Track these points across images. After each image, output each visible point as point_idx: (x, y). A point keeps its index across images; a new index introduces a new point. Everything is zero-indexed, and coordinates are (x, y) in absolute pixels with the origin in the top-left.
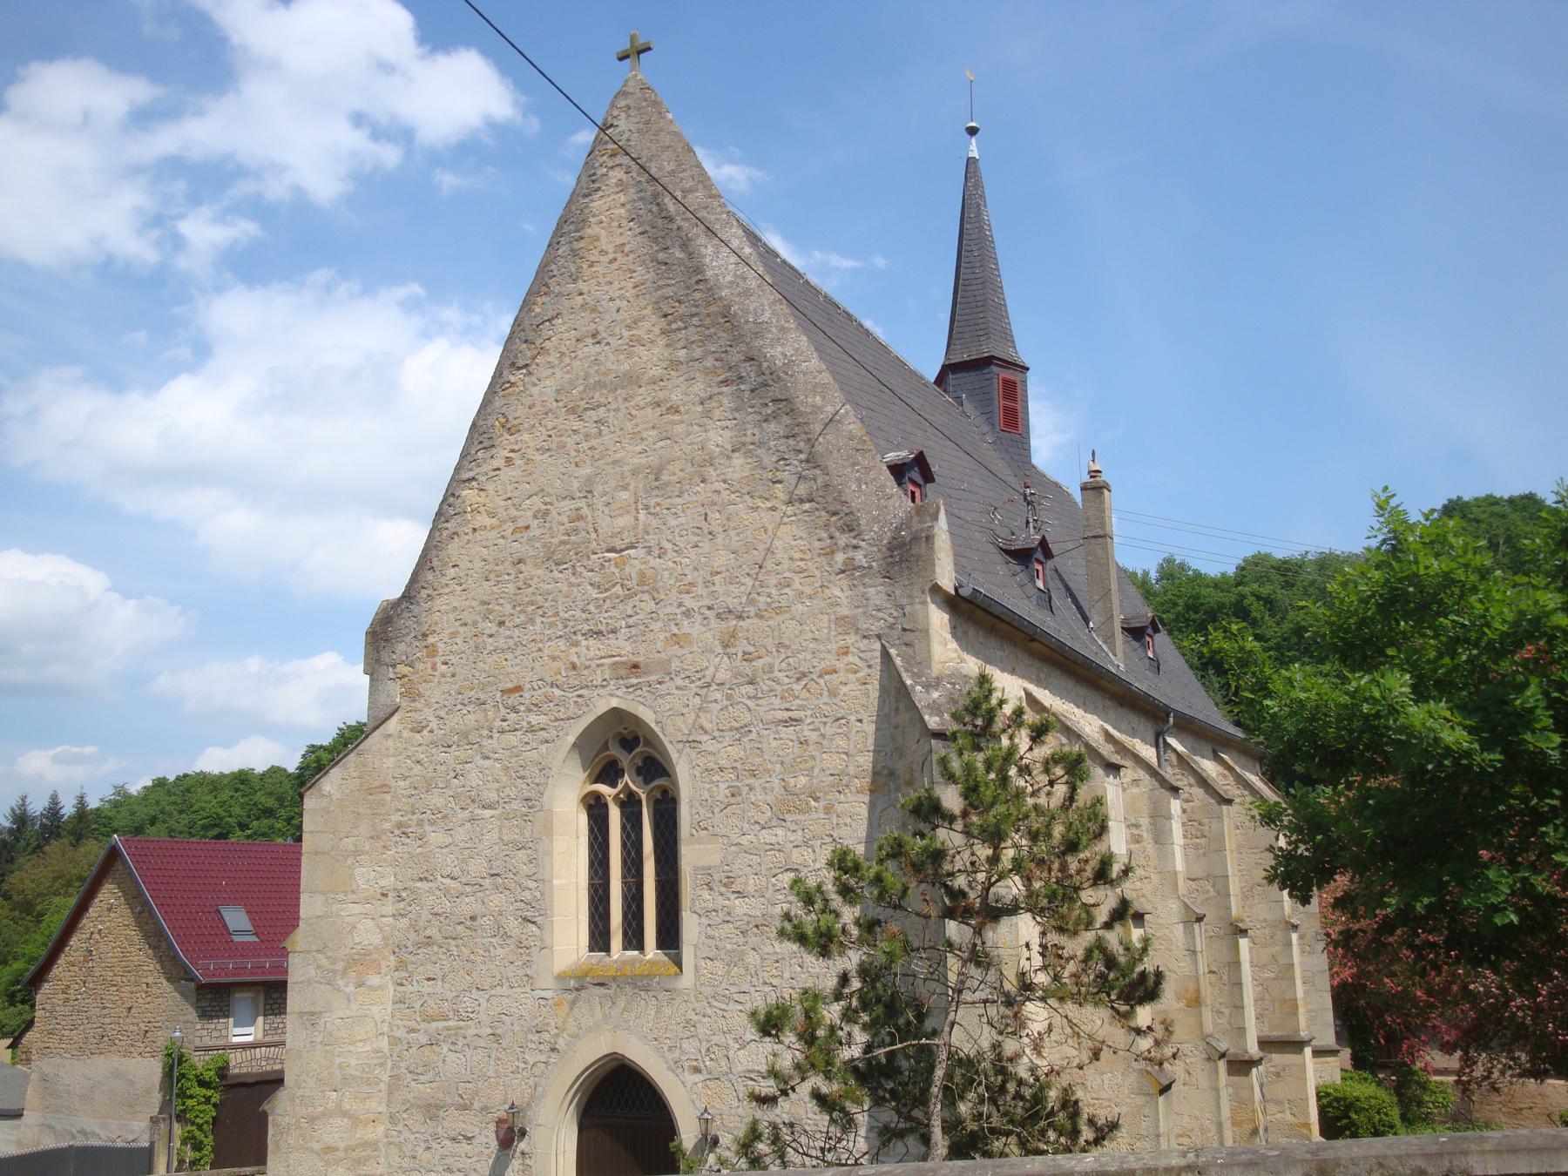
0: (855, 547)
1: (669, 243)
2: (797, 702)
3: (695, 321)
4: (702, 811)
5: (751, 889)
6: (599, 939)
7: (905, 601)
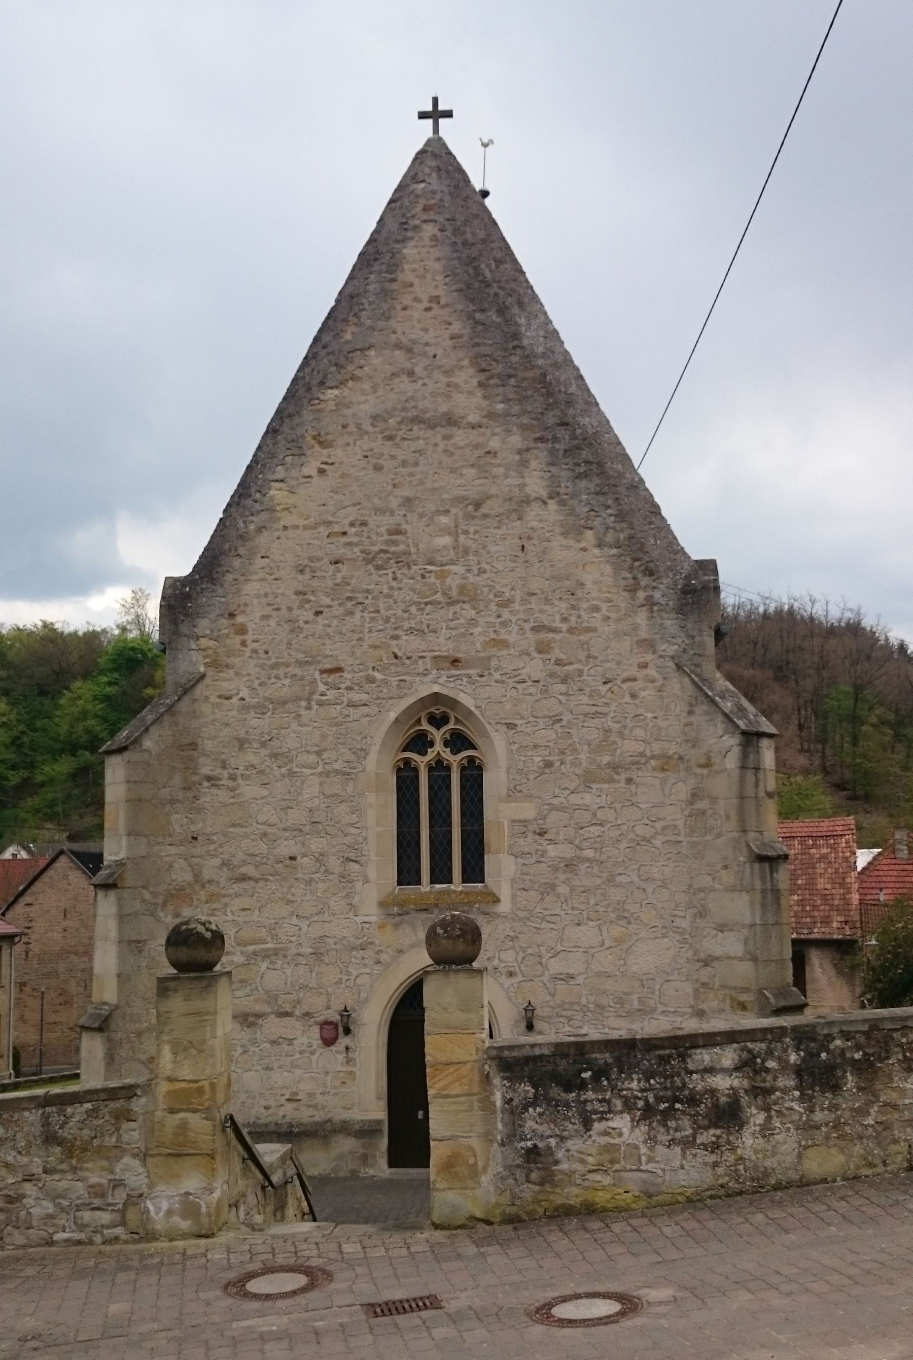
0: (654, 588)
1: (486, 306)
2: (603, 700)
3: (512, 381)
4: (518, 778)
5: (561, 838)
6: (407, 873)
7: (695, 633)
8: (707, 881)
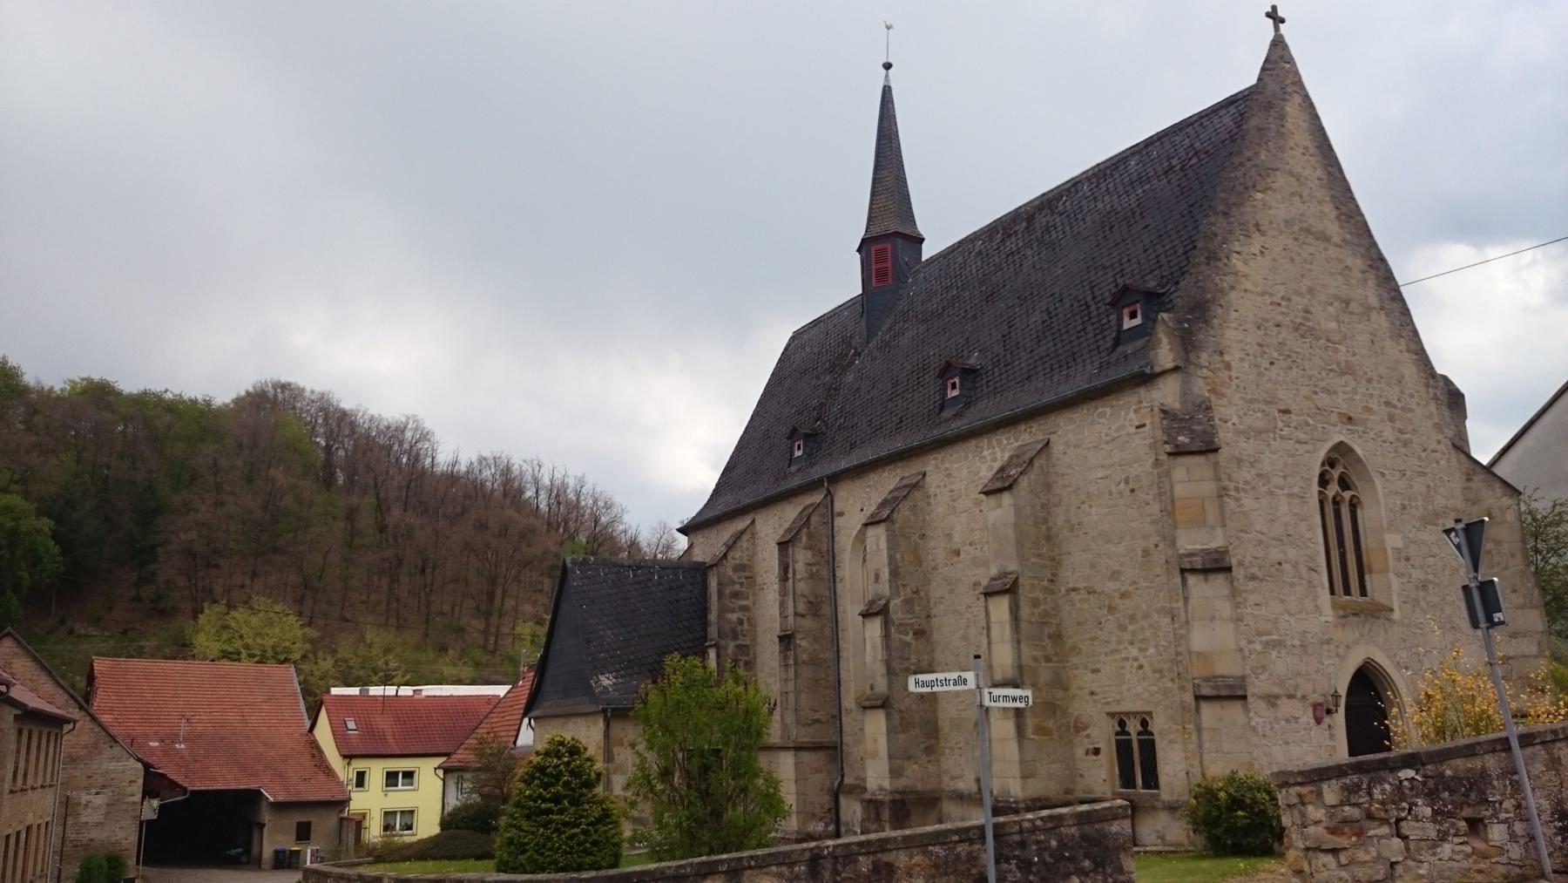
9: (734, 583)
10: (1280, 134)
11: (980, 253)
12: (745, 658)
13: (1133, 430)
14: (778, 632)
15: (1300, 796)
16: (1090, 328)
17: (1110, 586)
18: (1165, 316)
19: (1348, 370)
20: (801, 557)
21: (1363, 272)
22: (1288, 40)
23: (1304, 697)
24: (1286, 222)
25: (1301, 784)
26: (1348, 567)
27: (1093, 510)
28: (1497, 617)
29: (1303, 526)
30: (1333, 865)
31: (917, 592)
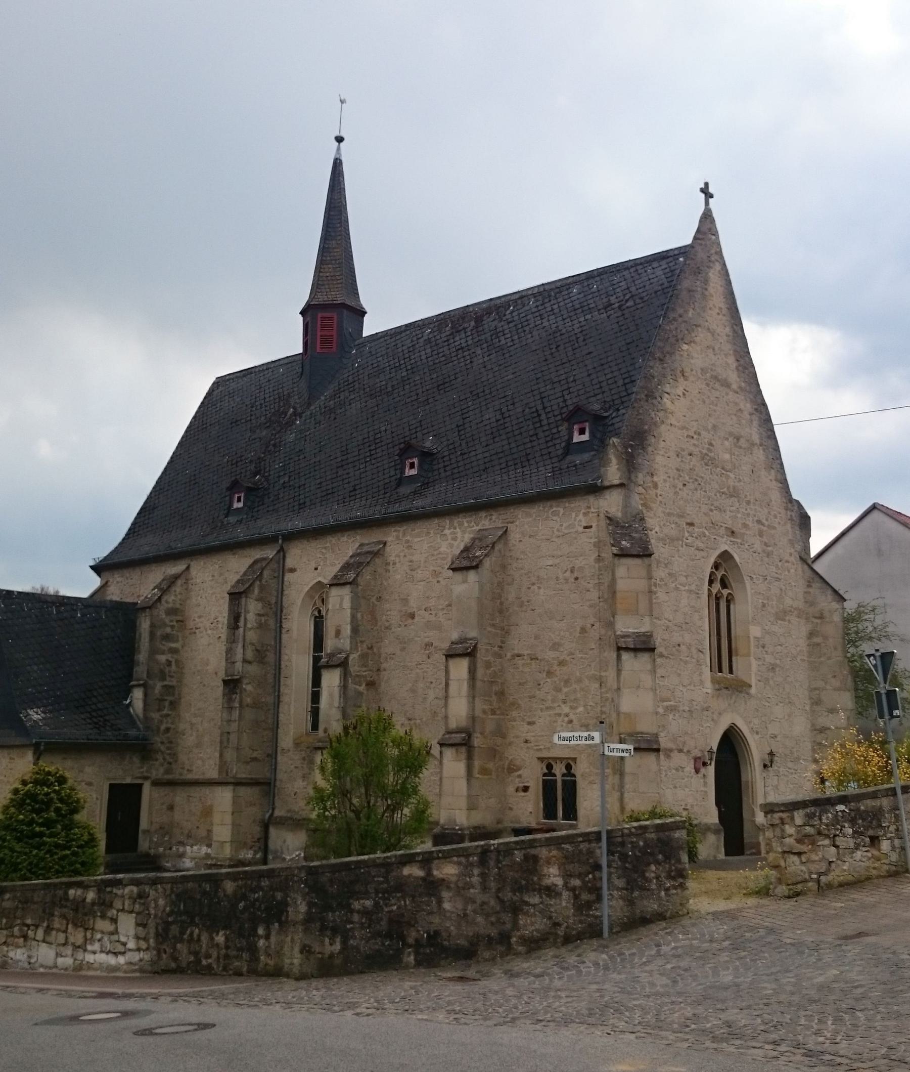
8: (820, 684)
9: (165, 625)
10: (704, 296)
11: (429, 341)
12: (170, 698)
13: (581, 529)
14: (222, 675)
15: (781, 819)
16: (541, 435)
17: (551, 655)
18: (615, 440)
19: (734, 493)
20: (252, 608)
21: (751, 414)
22: (715, 215)
23: (689, 751)
24: (702, 370)
25: (782, 811)
26: (724, 651)
27: (542, 591)
28: (896, 712)
29: (696, 616)
30: (798, 863)
31: (371, 648)
